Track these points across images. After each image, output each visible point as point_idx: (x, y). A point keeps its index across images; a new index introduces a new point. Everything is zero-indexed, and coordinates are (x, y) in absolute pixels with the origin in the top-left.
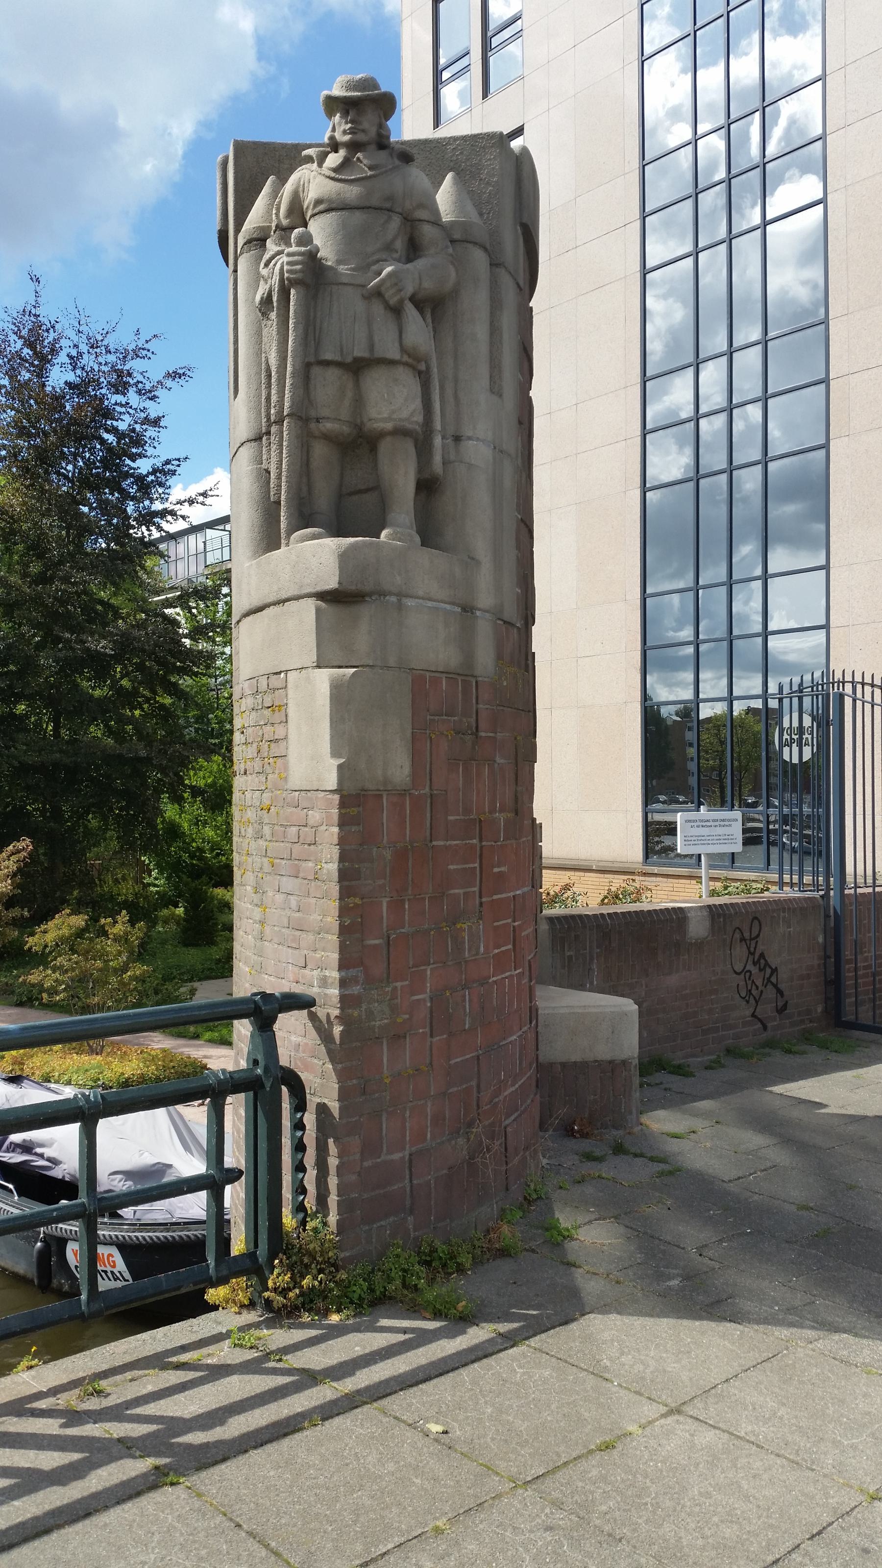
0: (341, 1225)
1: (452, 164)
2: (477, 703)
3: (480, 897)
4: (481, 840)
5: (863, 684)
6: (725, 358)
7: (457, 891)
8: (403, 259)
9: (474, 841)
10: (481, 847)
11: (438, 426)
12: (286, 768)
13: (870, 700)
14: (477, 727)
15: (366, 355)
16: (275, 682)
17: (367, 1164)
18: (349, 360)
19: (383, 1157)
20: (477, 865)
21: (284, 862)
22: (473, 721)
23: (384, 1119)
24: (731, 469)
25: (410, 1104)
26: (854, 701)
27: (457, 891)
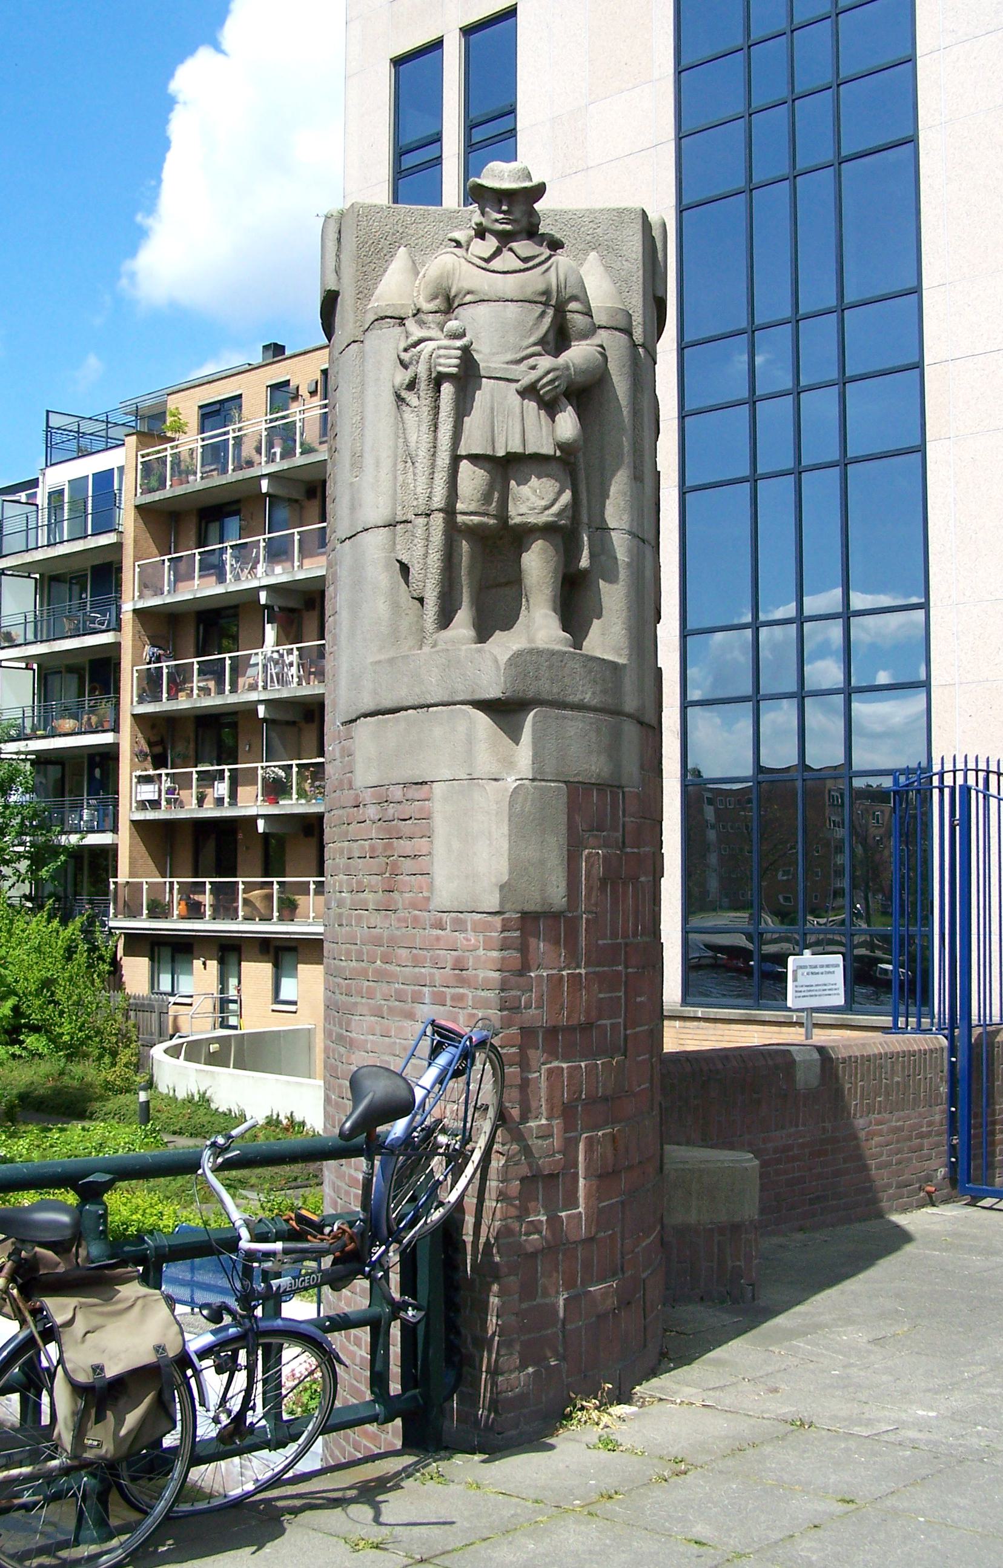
0: (599, 1217)
1: (588, 238)
2: (624, 816)
3: (625, 1030)
4: (626, 967)
5: (988, 772)
6: (834, 317)
7: (604, 1022)
8: (553, 352)
9: (620, 968)
10: (627, 975)
11: (585, 519)
12: (431, 886)
13: (996, 794)
14: (624, 843)
15: (520, 450)
16: (413, 792)
17: (524, 1306)
18: (501, 453)
19: (539, 1300)
20: (622, 994)
21: (426, 989)
22: (619, 834)
23: (539, 1262)
24: (954, 772)
25: (562, 1247)
26: (986, 797)
27: (604, 1022)
